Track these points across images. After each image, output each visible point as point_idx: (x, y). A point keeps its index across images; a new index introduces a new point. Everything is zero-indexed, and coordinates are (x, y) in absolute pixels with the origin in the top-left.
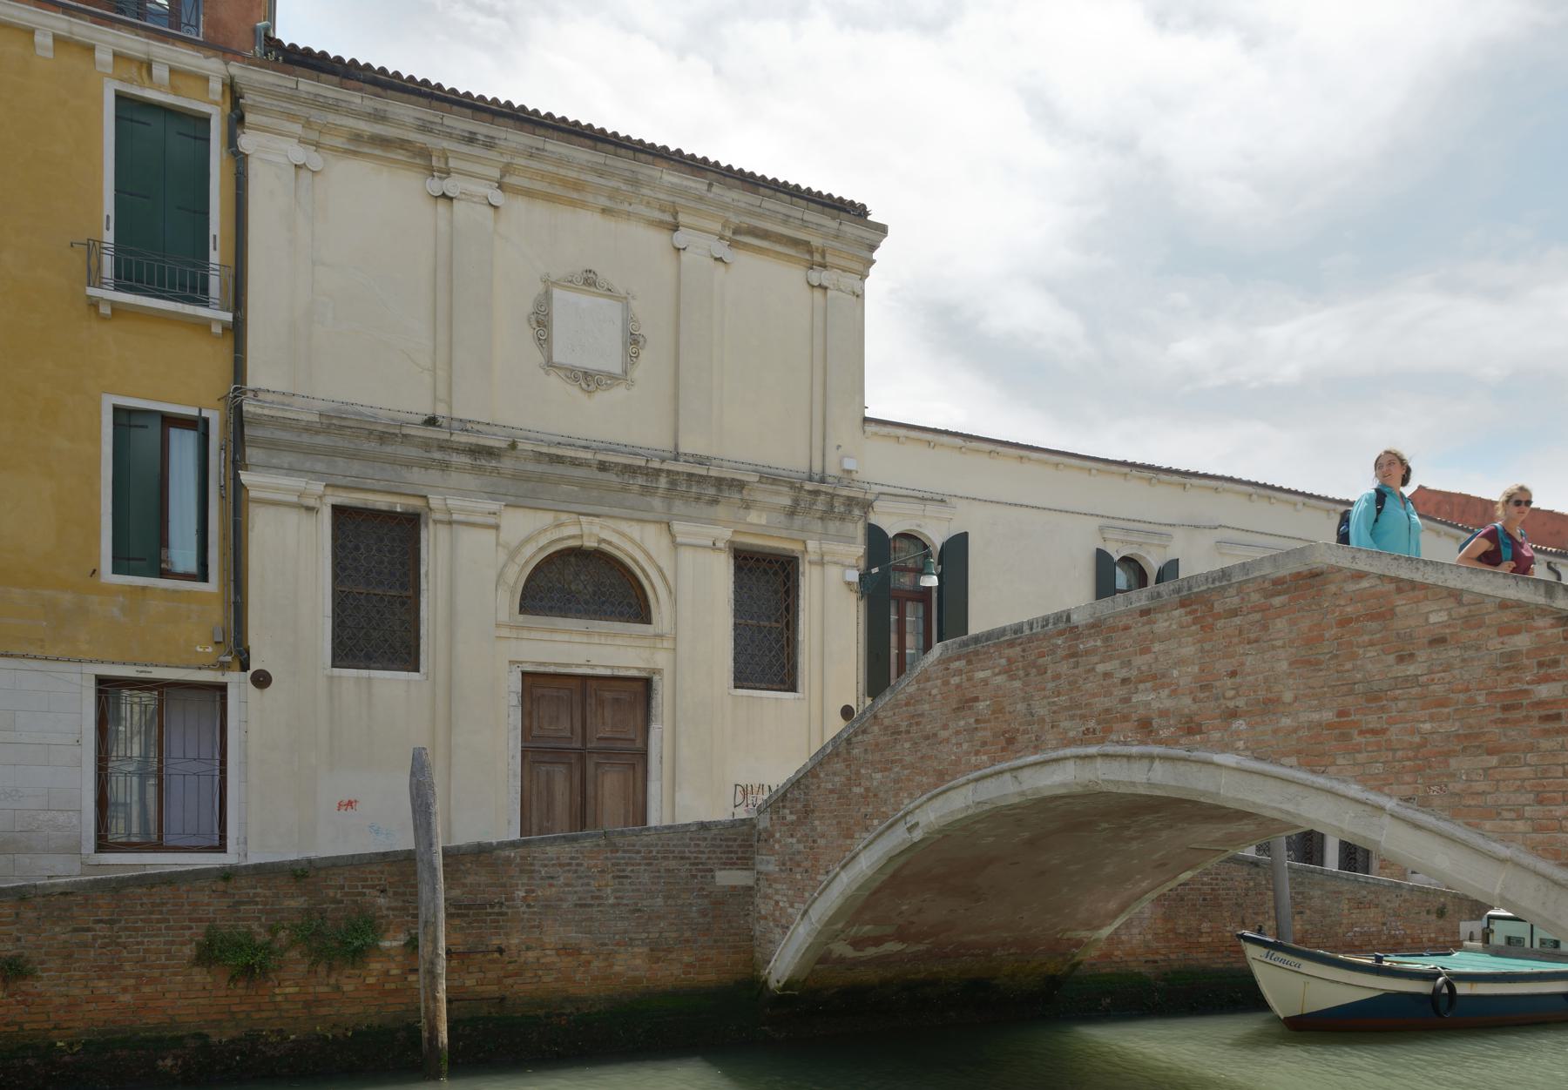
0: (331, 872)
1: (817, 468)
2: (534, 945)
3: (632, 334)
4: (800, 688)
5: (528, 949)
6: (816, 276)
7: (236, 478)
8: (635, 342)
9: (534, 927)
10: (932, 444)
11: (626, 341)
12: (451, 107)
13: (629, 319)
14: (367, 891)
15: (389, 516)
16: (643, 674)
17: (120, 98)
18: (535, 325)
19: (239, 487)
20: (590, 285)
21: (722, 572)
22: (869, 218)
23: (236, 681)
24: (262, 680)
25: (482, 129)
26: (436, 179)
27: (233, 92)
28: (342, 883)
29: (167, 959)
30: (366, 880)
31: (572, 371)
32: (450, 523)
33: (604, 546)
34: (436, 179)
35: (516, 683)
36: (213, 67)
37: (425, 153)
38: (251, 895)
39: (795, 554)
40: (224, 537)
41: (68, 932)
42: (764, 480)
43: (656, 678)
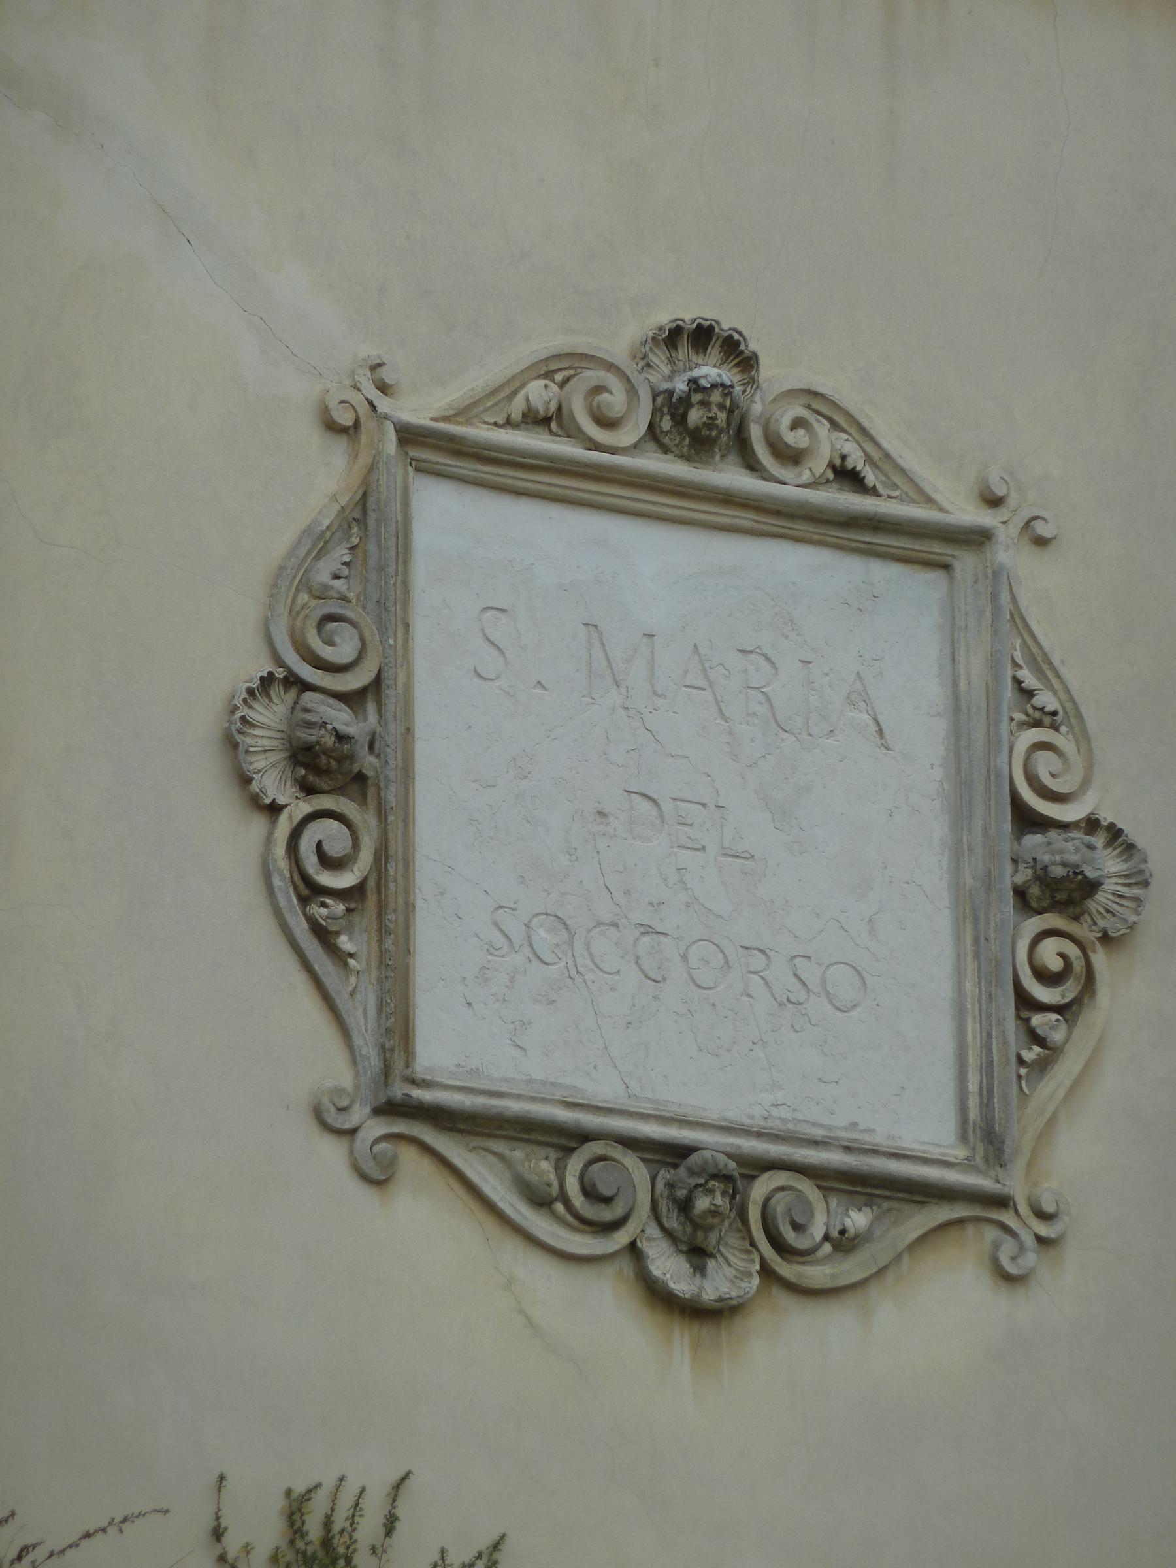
11: (989, 882)
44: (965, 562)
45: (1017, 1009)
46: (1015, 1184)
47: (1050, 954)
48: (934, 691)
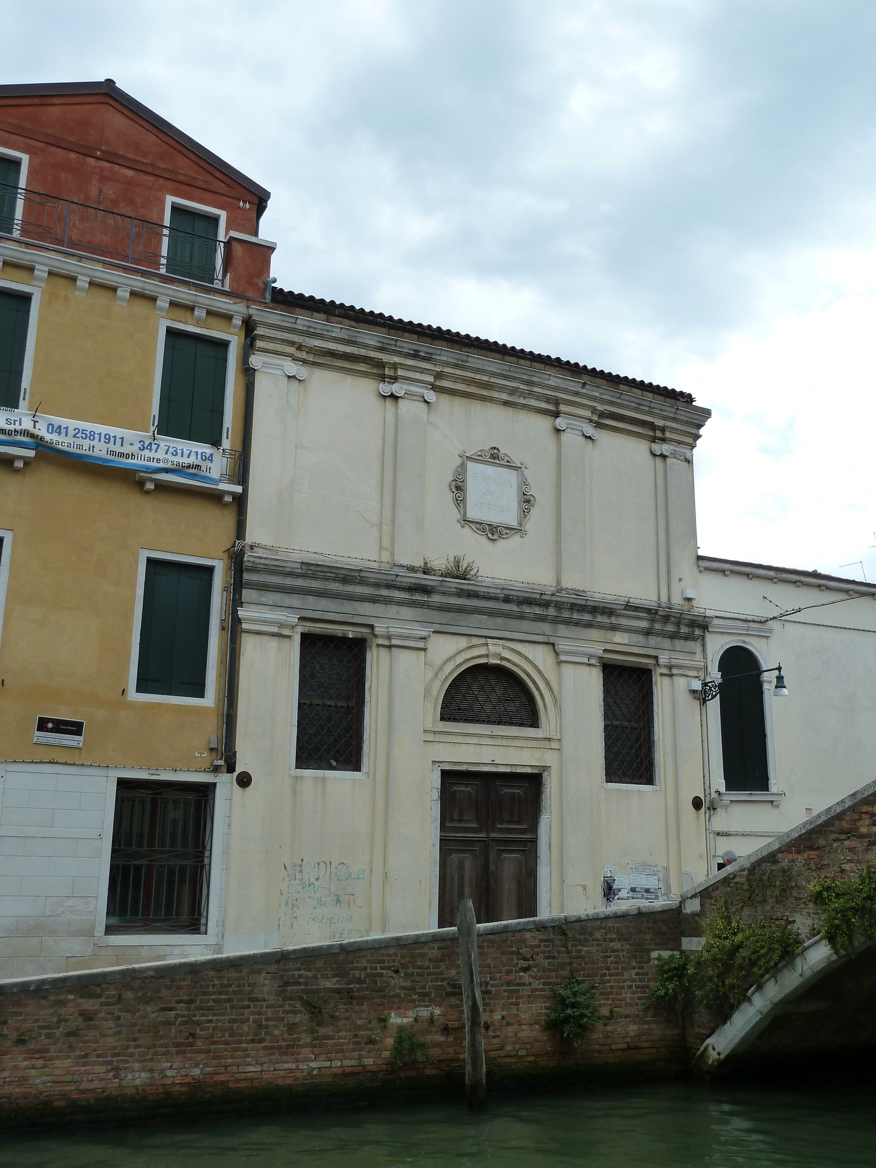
0: (357, 955)
1: (664, 599)
2: (512, 1021)
3: (524, 494)
4: (657, 781)
5: (508, 1024)
6: (657, 448)
7: (234, 613)
8: (528, 501)
9: (512, 1004)
10: (751, 576)
11: (521, 500)
12: (403, 334)
13: (524, 482)
14: (384, 972)
15: (343, 641)
16: (535, 771)
17: (170, 332)
18: (454, 490)
19: (236, 621)
20: (494, 458)
21: (594, 680)
22: (694, 403)
23: (225, 784)
24: (244, 781)
25: (424, 347)
26: (386, 383)
27: (249, 326)
28: (365, 965)
29: (230, 1036)
30: (383, 962)
31: (481, 524)
32: (390, 647)
33: (505, 663)
34: (386, 383)
35: (436, 780)
36: (238, 309)
37: (381, 365)
38: (296, 976)
39: (649, 667)
40: (222, 661)
41: (156, 1011)
42: (628, 608)
43: (545, 775)
44: (519, 470)
45: (200, 933)
46: (523, 529)
47: (526, 507)
48: (516, 483)
